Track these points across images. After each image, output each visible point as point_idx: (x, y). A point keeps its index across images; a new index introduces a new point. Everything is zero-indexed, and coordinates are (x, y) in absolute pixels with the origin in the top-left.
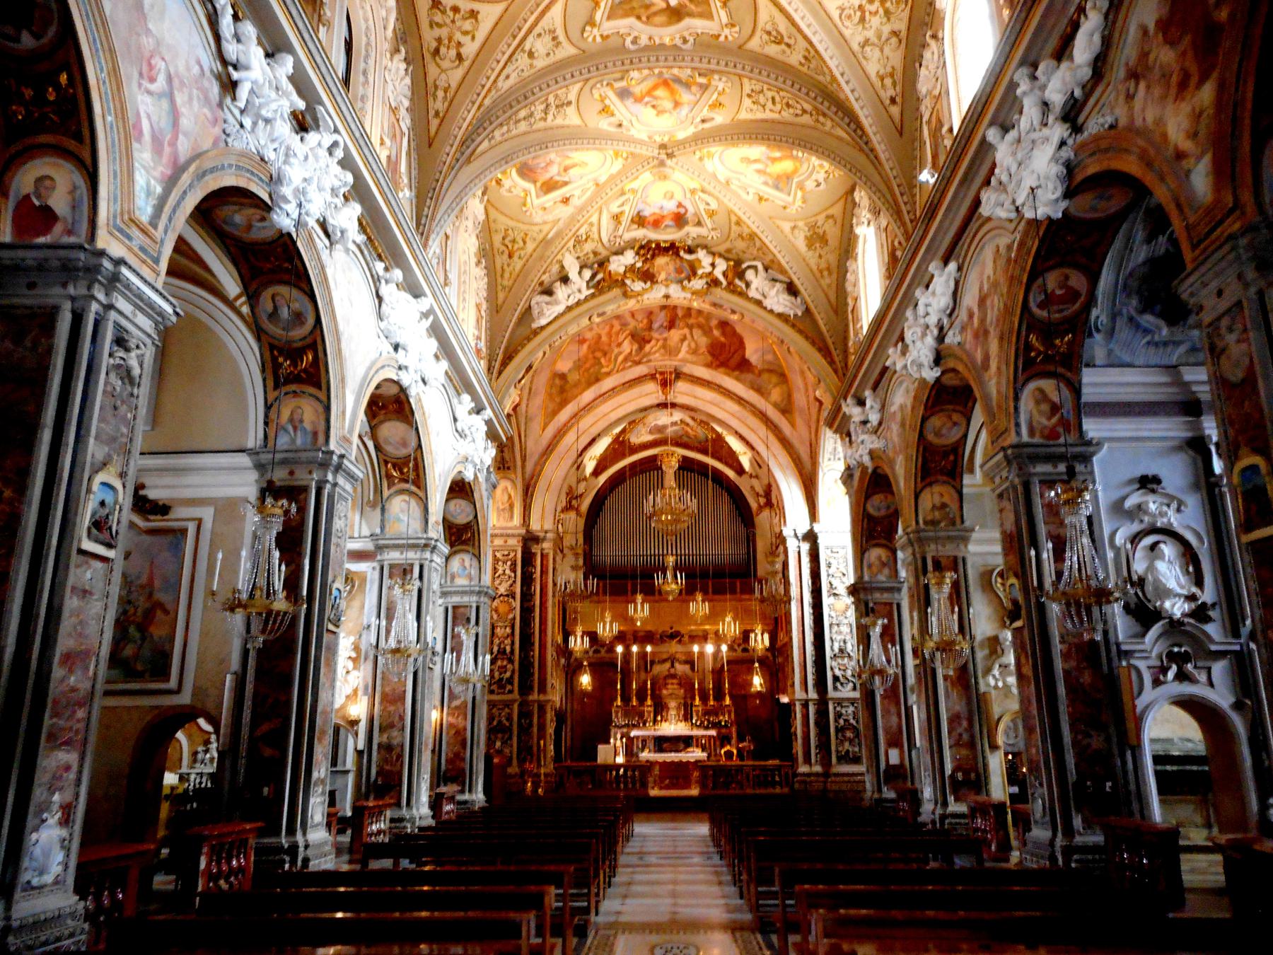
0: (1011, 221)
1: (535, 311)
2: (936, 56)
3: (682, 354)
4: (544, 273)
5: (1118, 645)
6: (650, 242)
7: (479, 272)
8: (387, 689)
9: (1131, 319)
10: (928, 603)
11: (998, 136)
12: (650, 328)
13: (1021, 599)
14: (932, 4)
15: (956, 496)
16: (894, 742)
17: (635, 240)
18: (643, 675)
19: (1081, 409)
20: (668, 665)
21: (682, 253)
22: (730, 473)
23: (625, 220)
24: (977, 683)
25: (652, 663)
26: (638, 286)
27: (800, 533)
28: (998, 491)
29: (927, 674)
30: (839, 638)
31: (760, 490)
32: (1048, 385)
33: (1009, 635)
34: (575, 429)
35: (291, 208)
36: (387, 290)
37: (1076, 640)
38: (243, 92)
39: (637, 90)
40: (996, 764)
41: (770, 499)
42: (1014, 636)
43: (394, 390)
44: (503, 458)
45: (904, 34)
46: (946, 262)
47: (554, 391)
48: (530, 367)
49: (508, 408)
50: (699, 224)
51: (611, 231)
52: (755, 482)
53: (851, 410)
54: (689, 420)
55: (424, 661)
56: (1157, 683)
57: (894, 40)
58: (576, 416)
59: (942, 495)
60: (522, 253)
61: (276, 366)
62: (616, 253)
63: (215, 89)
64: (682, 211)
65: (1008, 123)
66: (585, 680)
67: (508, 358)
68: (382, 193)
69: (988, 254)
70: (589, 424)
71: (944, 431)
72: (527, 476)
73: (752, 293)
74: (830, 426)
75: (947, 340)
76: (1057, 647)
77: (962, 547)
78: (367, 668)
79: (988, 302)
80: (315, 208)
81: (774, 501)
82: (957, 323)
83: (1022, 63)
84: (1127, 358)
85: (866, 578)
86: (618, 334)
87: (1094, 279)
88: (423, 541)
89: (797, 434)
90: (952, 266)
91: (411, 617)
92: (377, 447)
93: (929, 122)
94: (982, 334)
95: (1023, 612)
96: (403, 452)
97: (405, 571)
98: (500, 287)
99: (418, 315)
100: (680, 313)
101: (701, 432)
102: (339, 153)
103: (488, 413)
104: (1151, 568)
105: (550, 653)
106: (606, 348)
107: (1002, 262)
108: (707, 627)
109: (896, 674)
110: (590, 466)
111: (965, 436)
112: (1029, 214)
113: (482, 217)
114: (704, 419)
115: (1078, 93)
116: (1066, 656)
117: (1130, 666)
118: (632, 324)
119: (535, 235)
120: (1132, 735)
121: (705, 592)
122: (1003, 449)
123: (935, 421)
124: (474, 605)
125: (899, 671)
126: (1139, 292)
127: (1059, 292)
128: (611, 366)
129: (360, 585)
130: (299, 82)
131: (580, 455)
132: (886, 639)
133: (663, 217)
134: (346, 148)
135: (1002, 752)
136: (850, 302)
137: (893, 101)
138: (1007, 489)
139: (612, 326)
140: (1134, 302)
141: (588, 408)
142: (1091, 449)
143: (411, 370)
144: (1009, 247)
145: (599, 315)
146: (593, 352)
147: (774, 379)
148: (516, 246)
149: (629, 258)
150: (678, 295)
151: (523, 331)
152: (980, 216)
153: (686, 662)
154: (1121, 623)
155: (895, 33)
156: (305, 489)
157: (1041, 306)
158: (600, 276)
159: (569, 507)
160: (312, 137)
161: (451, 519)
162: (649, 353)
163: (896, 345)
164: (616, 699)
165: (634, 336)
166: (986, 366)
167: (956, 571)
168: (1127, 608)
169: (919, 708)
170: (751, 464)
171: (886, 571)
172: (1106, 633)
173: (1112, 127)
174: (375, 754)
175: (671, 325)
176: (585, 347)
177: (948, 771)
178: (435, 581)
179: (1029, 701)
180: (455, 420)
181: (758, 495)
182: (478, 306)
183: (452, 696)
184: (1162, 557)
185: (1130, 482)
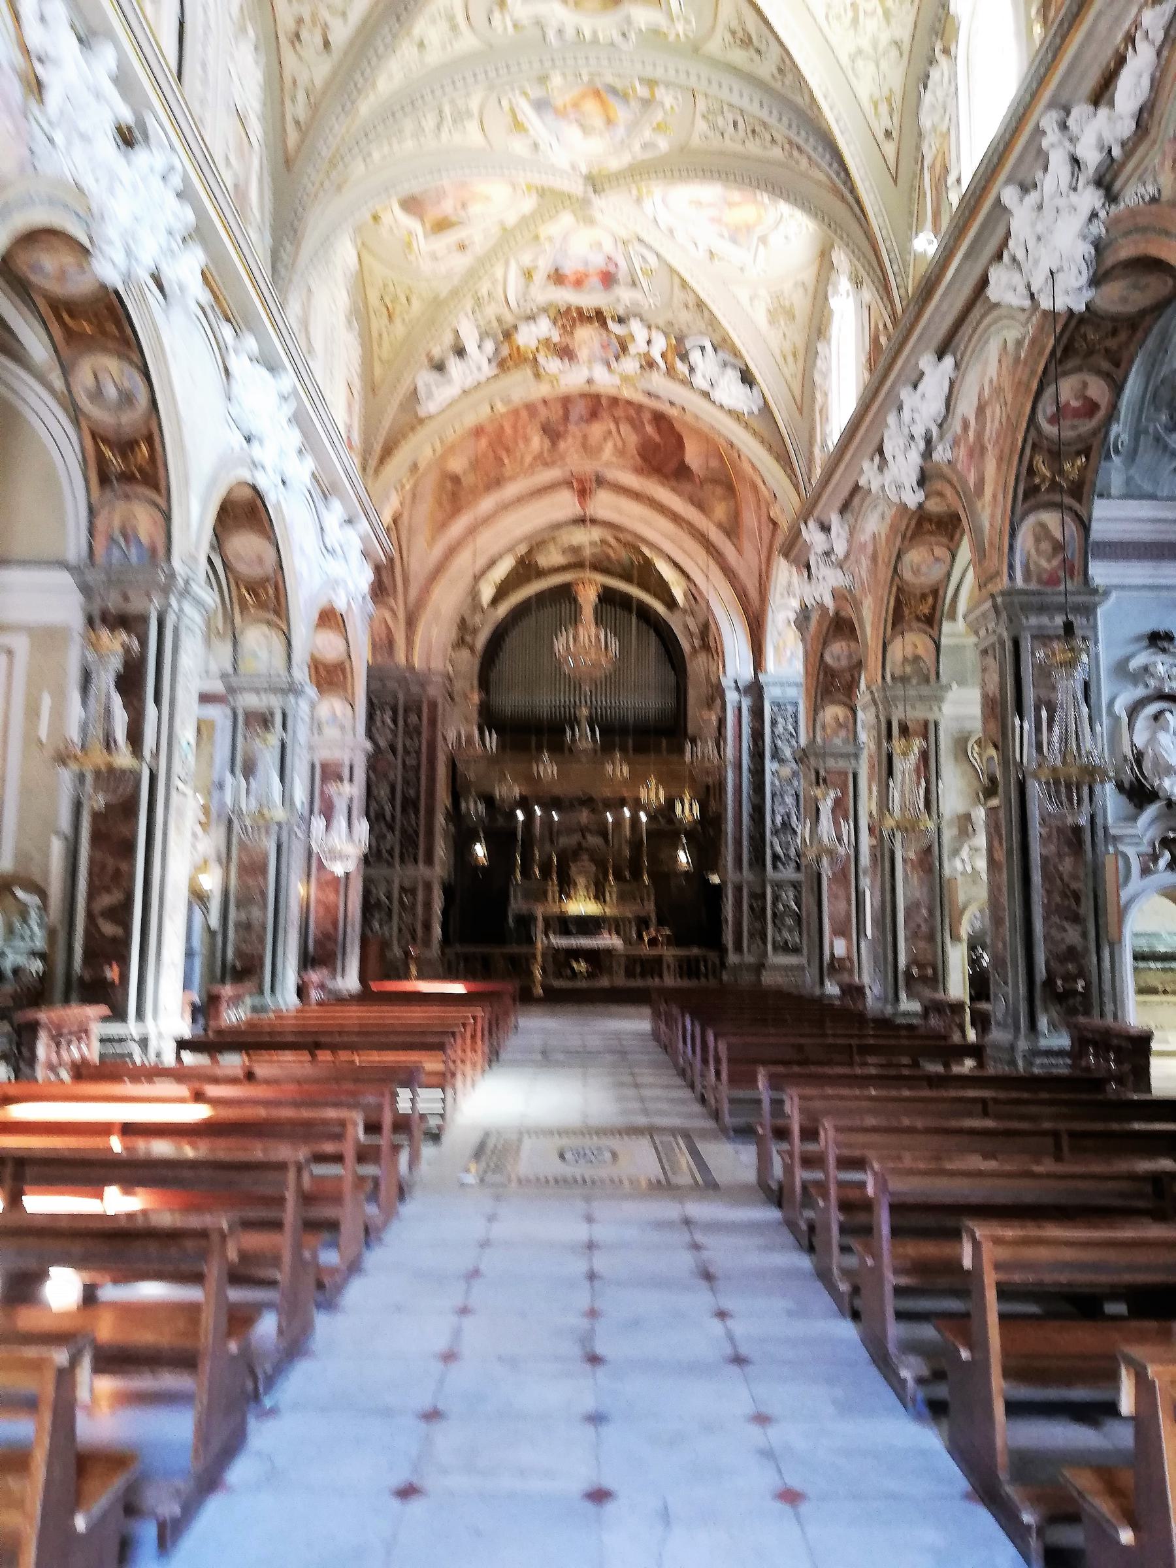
0: (1023, 310)
2: (946, 80)
5: (1105, 829)
9: (1158, 439)
10: (890, 773)
11: (1016, 198)
14: (945, 6)
16: (841, 931)
18: (547, 846)
19: (1090, 549)
21: (610, 323)
22: (660, 608)
23: (539, 277)
25: (559, 833)
26: (551, 365)
28: (982, 647)
29: (884, 857)
31: (693, 627)
32: (1051, 519)
35: (119, 257)
36: (237, 364)
37: (1059, 823)
38: (53, 96)
39: (559, 101)
40: (957, 961)
41: (708, 640)
42: (987, 815)
43: (247, 493)
45: (906, 47)
46: (940, 355)
49: (387, 518)
53: (812, 535)
54: (613, 542)
56: (1145, 871)
57: (894, 53)
58: (472, 531)
61: (102, 464)
63: (15, 90)
64: (612, 269)
65: (1029, 181)
66: (480, 850)
67: (388, 451)
68: (227, 227)
69: (993, 349)
70: (490, 540)
71: (924, 569)
73: (699, 381)
74: (786, 555)
75: (936, 456)
76: (1036, 829)
78: (219, 833)
80: (148, 254)
81: (712, 644)
82: (949, 437)
83: (1052, 105)
84: (1148, 487)
85: (819, 740)
87: (1117, 388)
89: (745, 564)
90: (949, 361)
92: (225, 565)
93: (932, 167)
94: (978, 451)
95: (1000, 790)
97: (264, 720)
100: (604, 401)
101: (624, 555)
102: (176, 181)
104: (1153, 740)
105: (440, 820)
107: (1008, 361)
109: (848, 855)
110: (487, 592)
111: (949, 575)
112: (1045, 304)
115: (1117, 152)
116: (1045, 840)
117: (1118, 853)
118: (543, 412)
120: (1112, 929)
121: (624, 750)
123: (915, 556)
124: (347, 763)
125: (852, 853)
126: (1170, 406)
127: (1075, 404)
130: (123, 81)
132: (839, 813)
134: (186, 178)
135: (964, 946)
136: (819, 396)
137: (888, 134)
138: (993, 645)
140: (1164, 418)
141: (487, 520)
142: (1097, 599)
144: (1019, 343)
147: (719, 491)
149: (544, 328)
150: (605, 381)
154: (1110, 799)
155: (897, 44)
156: (144, 619)
157: (1054, 419)
160: (141, 156)
161: (317, 655)
168: (1120, 787)
170: (685, 595)
171: (843, 733)
172: (1092, 817)
173: (1154, 200)
178: (301, 732)
179: (1000, 890)
181: (691, 634)
184: (1165, 729)
185: (1138, 639)
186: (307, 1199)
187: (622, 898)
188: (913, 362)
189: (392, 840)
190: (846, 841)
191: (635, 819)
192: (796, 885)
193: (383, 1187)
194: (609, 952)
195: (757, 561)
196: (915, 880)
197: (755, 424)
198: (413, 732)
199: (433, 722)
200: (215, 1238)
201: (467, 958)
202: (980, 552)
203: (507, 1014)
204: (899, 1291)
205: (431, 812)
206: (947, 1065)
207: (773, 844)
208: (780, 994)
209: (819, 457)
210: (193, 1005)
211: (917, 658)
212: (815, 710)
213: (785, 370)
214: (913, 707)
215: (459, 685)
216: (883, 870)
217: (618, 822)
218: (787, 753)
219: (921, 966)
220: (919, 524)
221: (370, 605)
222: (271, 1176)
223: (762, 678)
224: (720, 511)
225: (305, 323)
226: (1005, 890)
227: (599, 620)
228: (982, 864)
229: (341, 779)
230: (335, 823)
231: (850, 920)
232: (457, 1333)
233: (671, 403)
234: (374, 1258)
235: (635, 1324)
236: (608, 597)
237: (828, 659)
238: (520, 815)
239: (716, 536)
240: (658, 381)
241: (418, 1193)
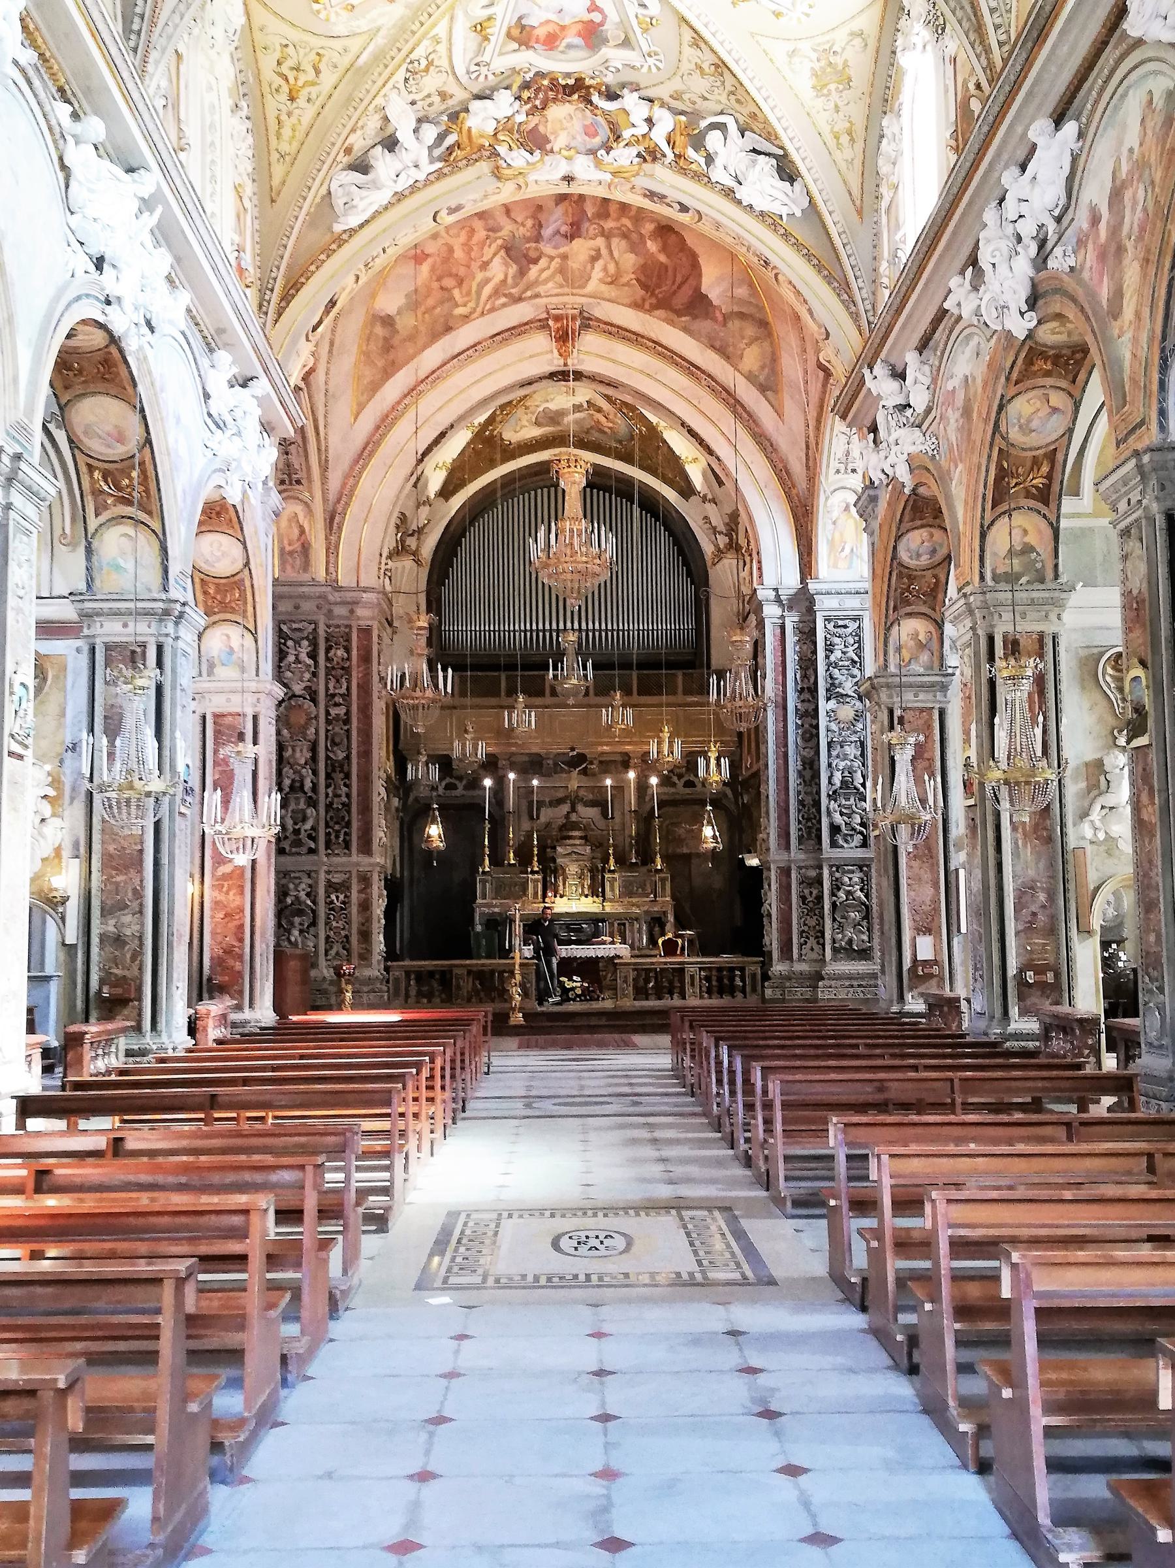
1: (338, 202)
3: (593, 286)
4: (353, 130)
6: (540, 75)
7: (237, 125)
8: (111, 848)
12: (538, 238)
13: (1147, 701)
15: (1048, 532)
17: (514, 71)
18: (526, 825)
20: (565, 808)
21: (595, 98)
22: (670, 494)
23: (497, 32)
24: (1063, 834)
25: (540, 804)
26: (518, 158)
27: (785, 594)
28: (1122, 525)
30: (842, 765)
31: (717, 521)
33: (1122, 759)
34: (412, 411)
43: (98, 339)
44: (288, 465)
46: (1059, 120)
47: (372, 347)
48: (332, 303)
49: (295, 379)
50: (626, 43)
51: (470, 55)
52: (710, 509)
53: (880, 384)
55: (171, 803)
58: (413, 392)
59: (1025, 532)
60: (314, 91)
62: (479, 97)
64: (596, 17)
66: (435, 831)
67: (292, 289)
72: (332, 497)
73: (718, 174)
74: (844, 417)
75: (1052, 263)
77: (1053, 616)
79: (1128, 195)
81: (742, 541)
86: (482, 245)
88: (161, 605)
90: (1070, 128)
91: (149, 731)
94: (1112, 253)
96: (118, 451)
97: (133, 656)
98: (275, 156)
99: (135, 205)
100: (590, 210)
101: (620, 424)
103: (262, 386)
105: (379, 790)
106: (462, 271)
108: (628, 748)
110: (435, 481)
111: (1071, 431)
113: (240, 20)
114: (628, 399)
118: (507, 228)
119: (336, 58)
121: (627, 692)
122: (1137, 454)
123: (1023, 407)
125: (940, 817)
128: (472, 305)
129: (56, 677)
131: (420, 461)
133: (563, 28)
135: (1097, 939)
139: (472, 231)
141: (433, 377)
143: (127, 303)
145: (452, 211)
146: (439, 279)
147: (750, 331)
148: (303, 78)
151: (318, 238)
152: (1125, 35)
153: (592, 804)
158: (451, 140)
159: (399, 551)
161: (205, 567)
162: (536, 283)
163: (962, 273)
164: (482, 863)
165: (508, 249)
166: (1115, 312)
167: (1041, 656)
169: (969, 874)
170: (704, 475)
171: (925, 657)
174: (95, 950)
175: (574, 232)
176: (425, 268)
177: (1012, 971)
178: (185, 672)
180: (207, 396)
181: (714, 530)
182: (238, 189)
183: (220, 860)
186: (193, 1322)
187: (628, 891)
188: (1019, 129)
189: (315, 817)
190: (931, 802)
191: (642, 787)
192: (862, 866)
193: (306, 1298)
194: (611, 962)
195: (802, 427)
196: (1028, 853)
197: (802, 233)
198: (338, 671)
199: (366, 658)
200: (47, 1396)
201: (421, 977)
202: (1117, 394)
203: (475, 1050)
204: (1050, 1432)
205: (366, 778)
206: (1083, 1108)
207: (832, 812)
208: (843, 1013)
209: (888, 274)
210: (46, 1053)
211: (1028, 549)
212: (886, 628)
213: (838, 155)
214: (1024, 616)
215: (401, 606)
216: (985, 838)
217: (619, 789)
218: (848, 687)
219: (1040, 970)
220: (1029, 362)
221: (275, 498)
222: (151, 1289)
223: (812, 586)
224: (752, 358)
225: (173, 103)
226: (1158, 861)
227: (588, 513)
228: (1122, 828)
229: (241, 737)
230: (236, 800)
231: (937, 910)
232: (416, 1506)
233: (684, 208)
234: (294, 1401)
235: (670, 1487)
236: (598, 482)
237: (904, 556)
238: (488, 782)
239: (748, 394)
240: (663, 178)
241: (356, 1301)
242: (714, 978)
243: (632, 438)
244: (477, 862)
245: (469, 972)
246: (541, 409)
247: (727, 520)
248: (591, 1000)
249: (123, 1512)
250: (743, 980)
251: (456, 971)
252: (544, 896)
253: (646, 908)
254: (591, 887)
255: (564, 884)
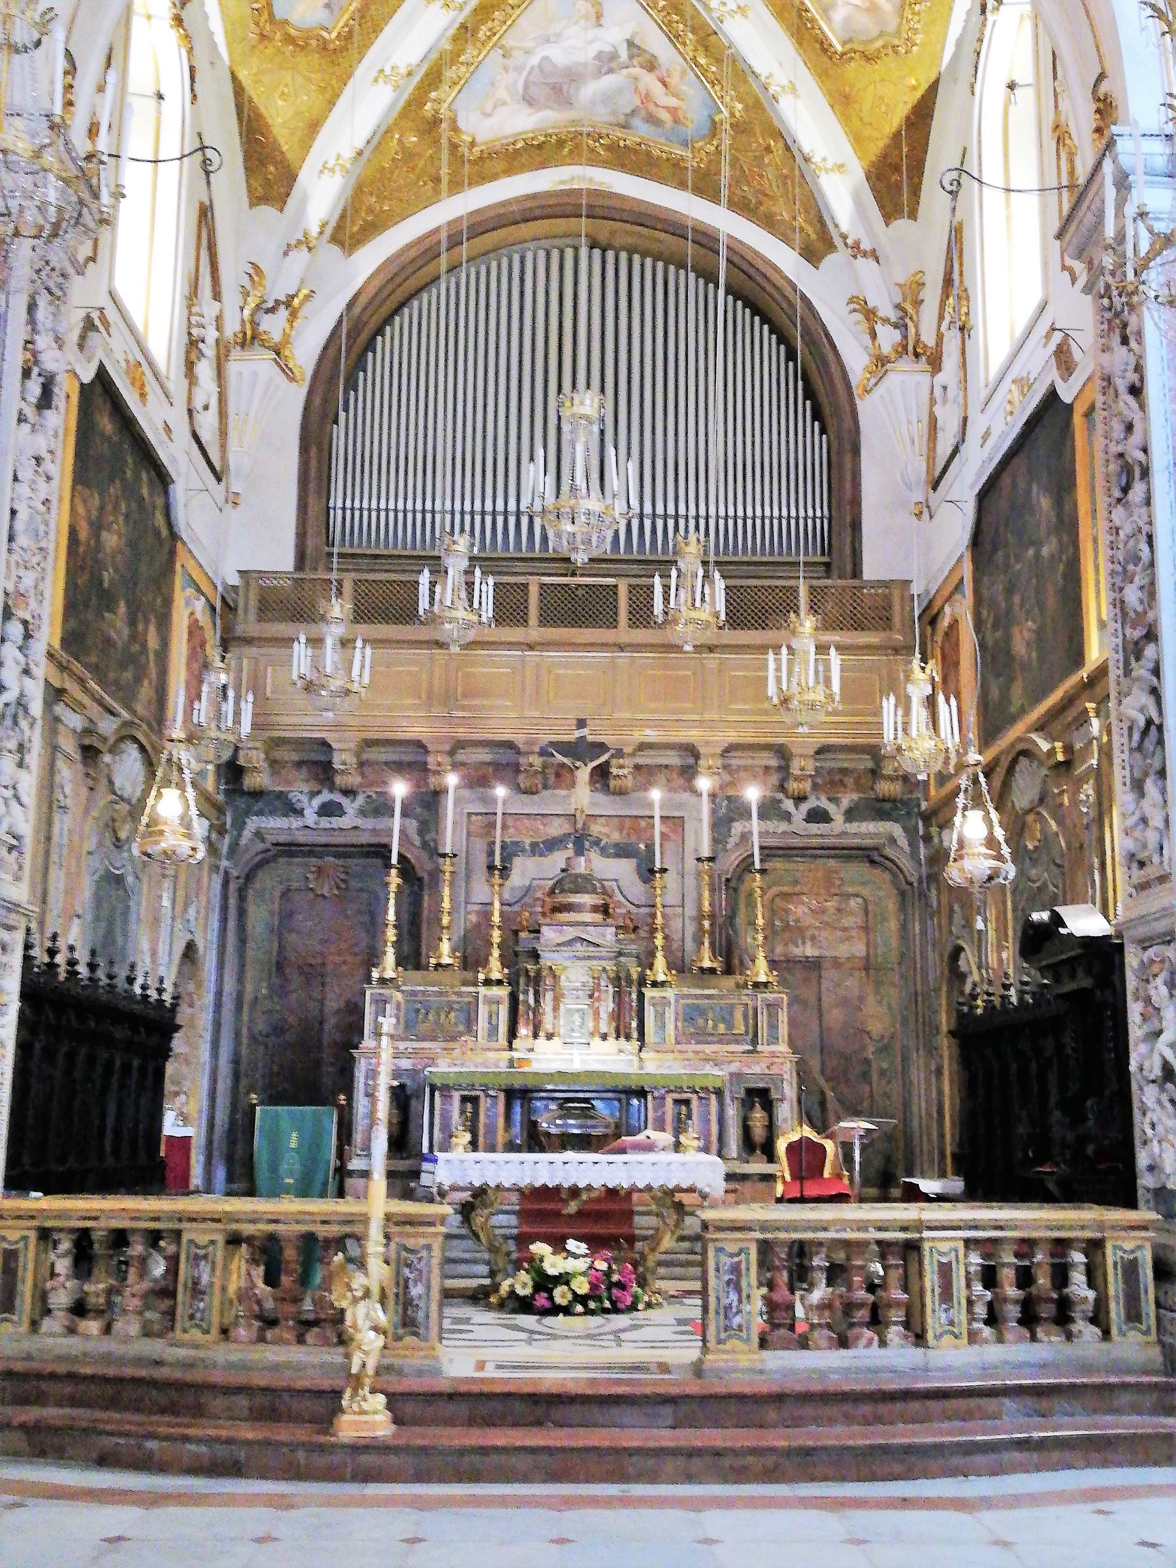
181: (870, 314)
242: (1007, 1276)
243: (714, 128)
244: (372, 958)
245: (234, 1240)
246: (534, 60)
247: (898, 299)
248: (615, 1310)
249: (627, 1075)
250: (1093, 1275)
251: (193, 1234)
252: (512, 1034)
253: (734, 1067)
254: (617, 1016)
255: (556, 1009)
